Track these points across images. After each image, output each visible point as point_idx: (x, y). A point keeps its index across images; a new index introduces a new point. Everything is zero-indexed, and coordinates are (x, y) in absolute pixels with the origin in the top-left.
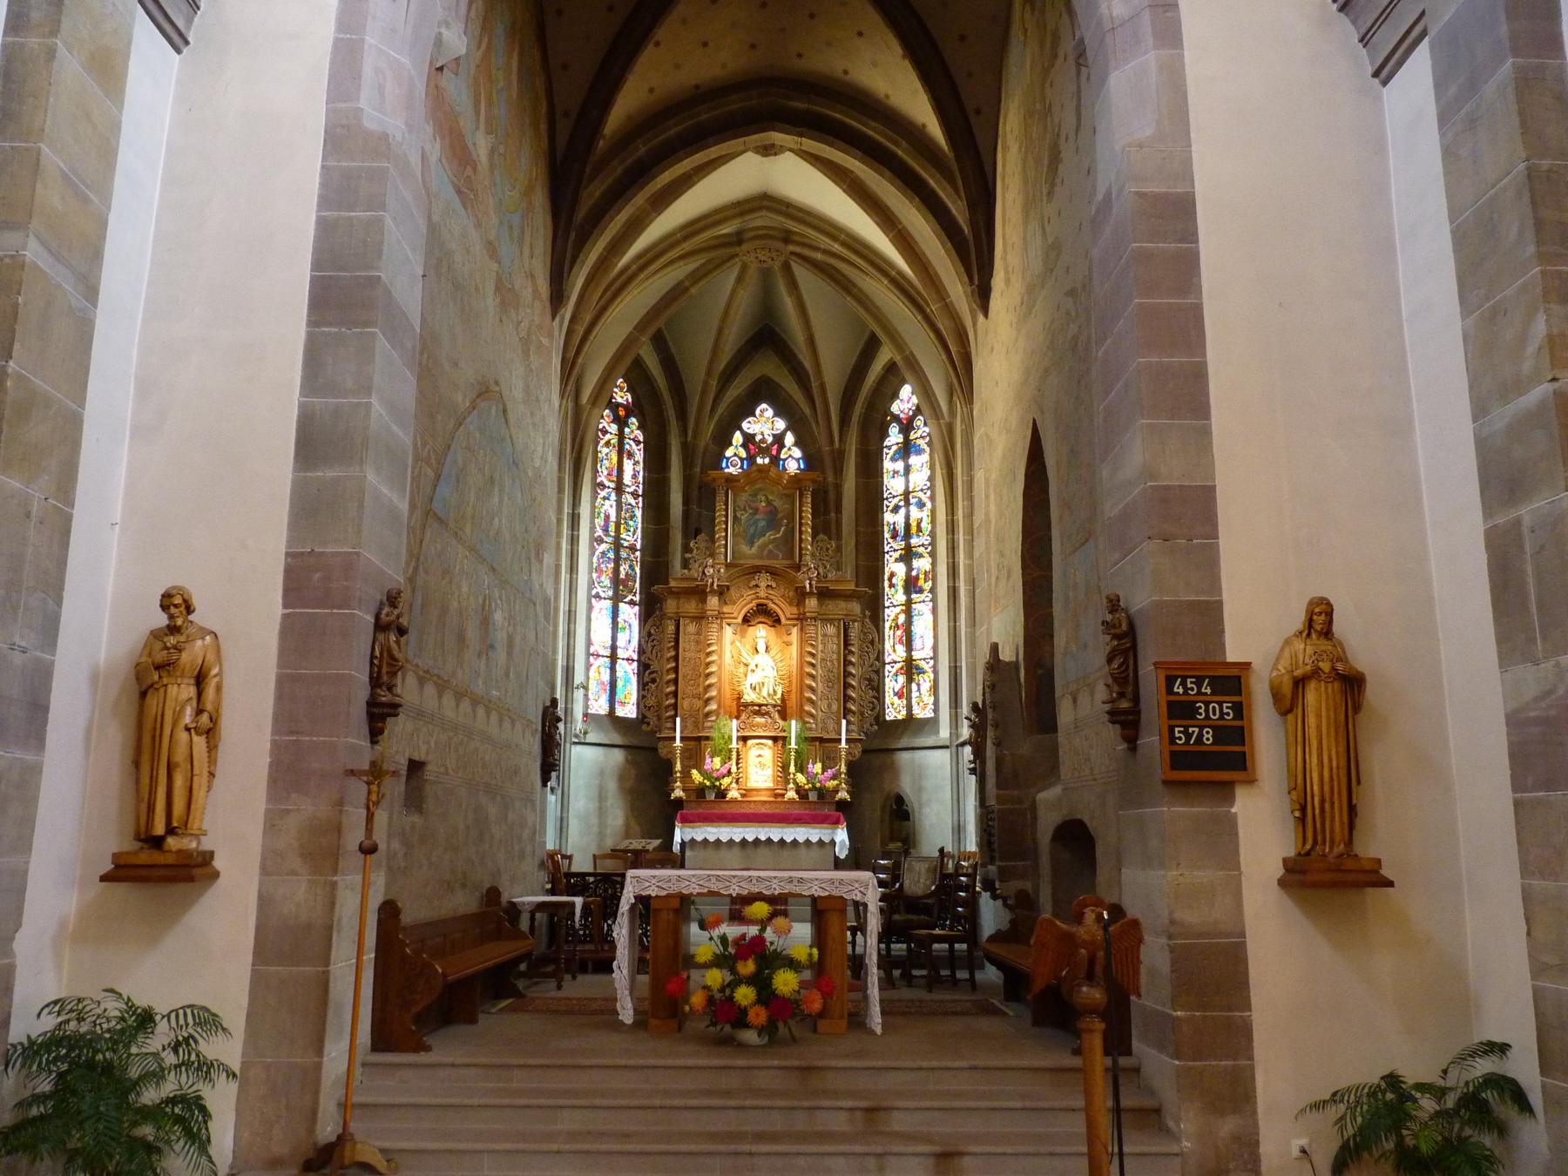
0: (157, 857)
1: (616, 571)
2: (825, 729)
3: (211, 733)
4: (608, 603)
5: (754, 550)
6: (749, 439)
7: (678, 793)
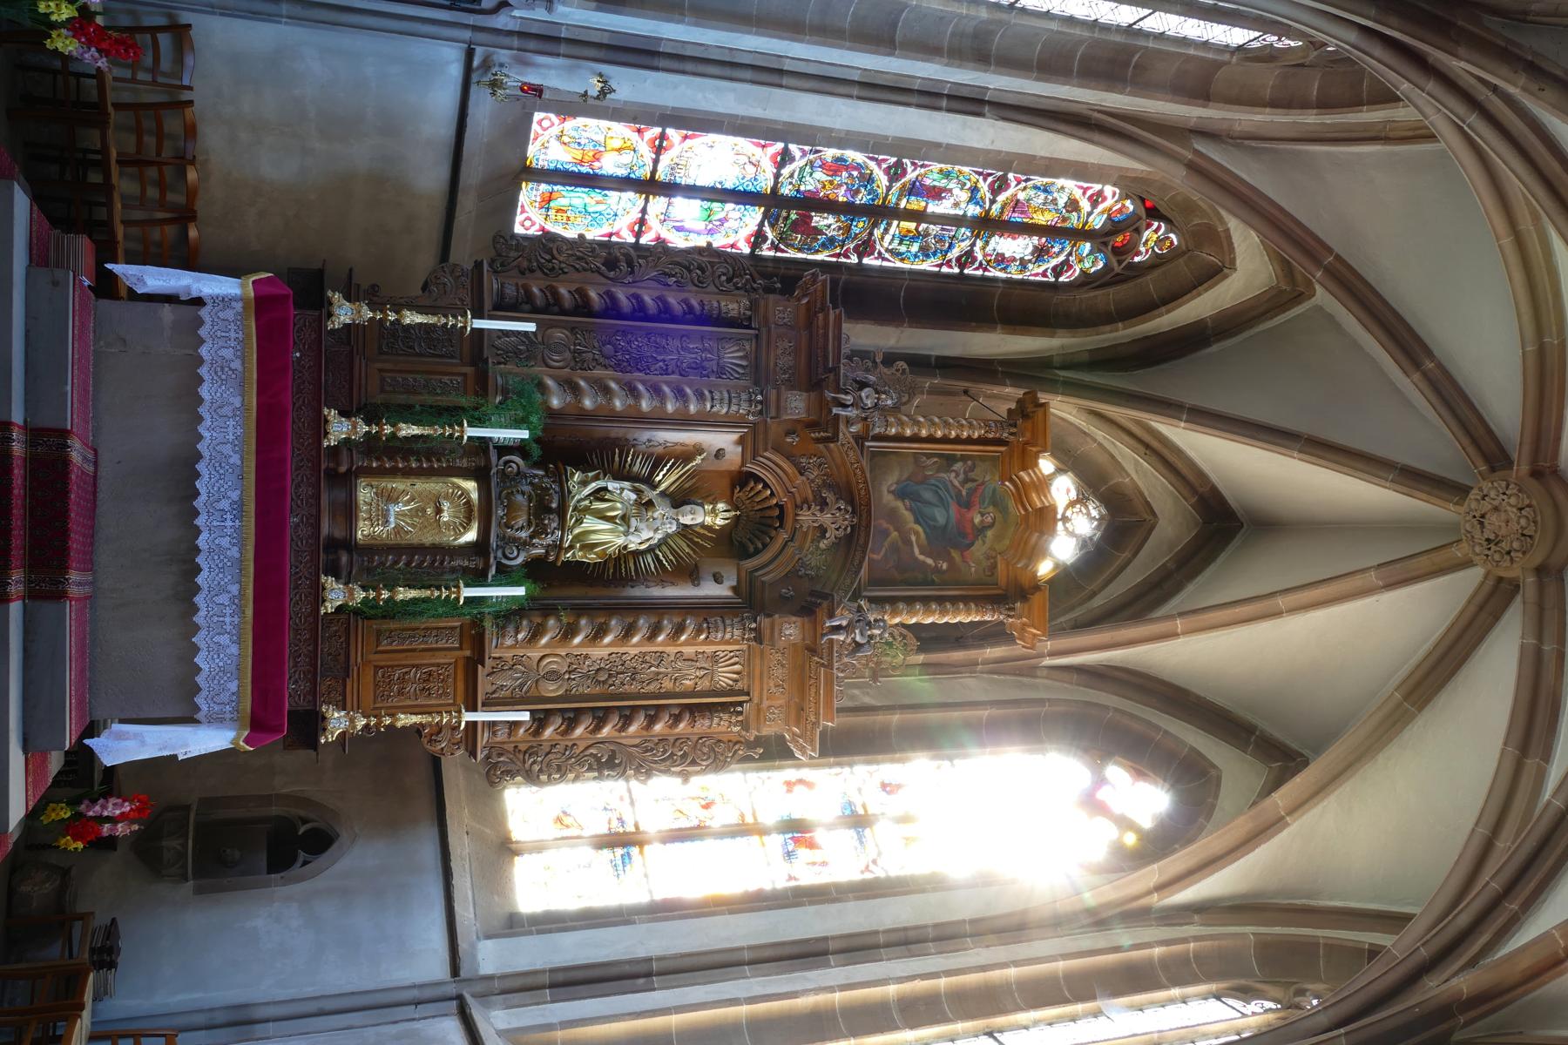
1: (829, 206)
2: (501, 667)
4: (765, 183)
5: (888, 498)
7: (339, 429)
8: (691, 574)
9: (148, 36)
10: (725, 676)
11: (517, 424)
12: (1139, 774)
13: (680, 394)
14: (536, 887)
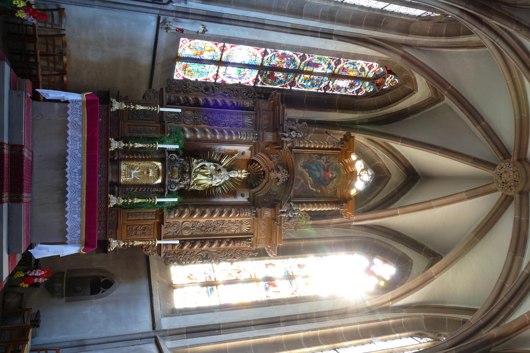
1: (280, 70)
2: (169, 225)
4: (259, 62)
5: (300, 168)
7: (115, 145)
8: (233, 194)
9: (50, 12)
10: (245, 228)
11: (175, 143)
12: (385, 261)
13: (230, 133)
14: (181, 299)
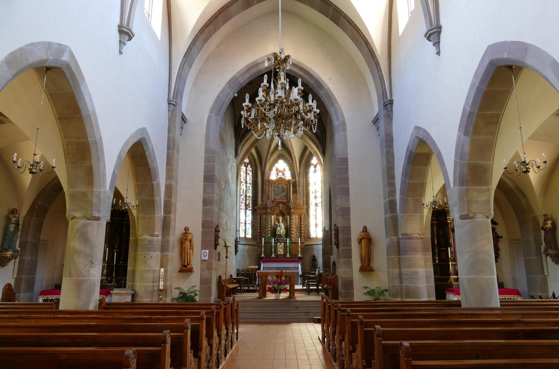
0: (186, 268)
1: (246, 203)
3: (192, 249)
6: (277, 170)
7: (273, 256)
8: (287, 220)
10: (297, 217)
